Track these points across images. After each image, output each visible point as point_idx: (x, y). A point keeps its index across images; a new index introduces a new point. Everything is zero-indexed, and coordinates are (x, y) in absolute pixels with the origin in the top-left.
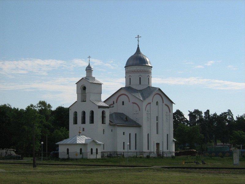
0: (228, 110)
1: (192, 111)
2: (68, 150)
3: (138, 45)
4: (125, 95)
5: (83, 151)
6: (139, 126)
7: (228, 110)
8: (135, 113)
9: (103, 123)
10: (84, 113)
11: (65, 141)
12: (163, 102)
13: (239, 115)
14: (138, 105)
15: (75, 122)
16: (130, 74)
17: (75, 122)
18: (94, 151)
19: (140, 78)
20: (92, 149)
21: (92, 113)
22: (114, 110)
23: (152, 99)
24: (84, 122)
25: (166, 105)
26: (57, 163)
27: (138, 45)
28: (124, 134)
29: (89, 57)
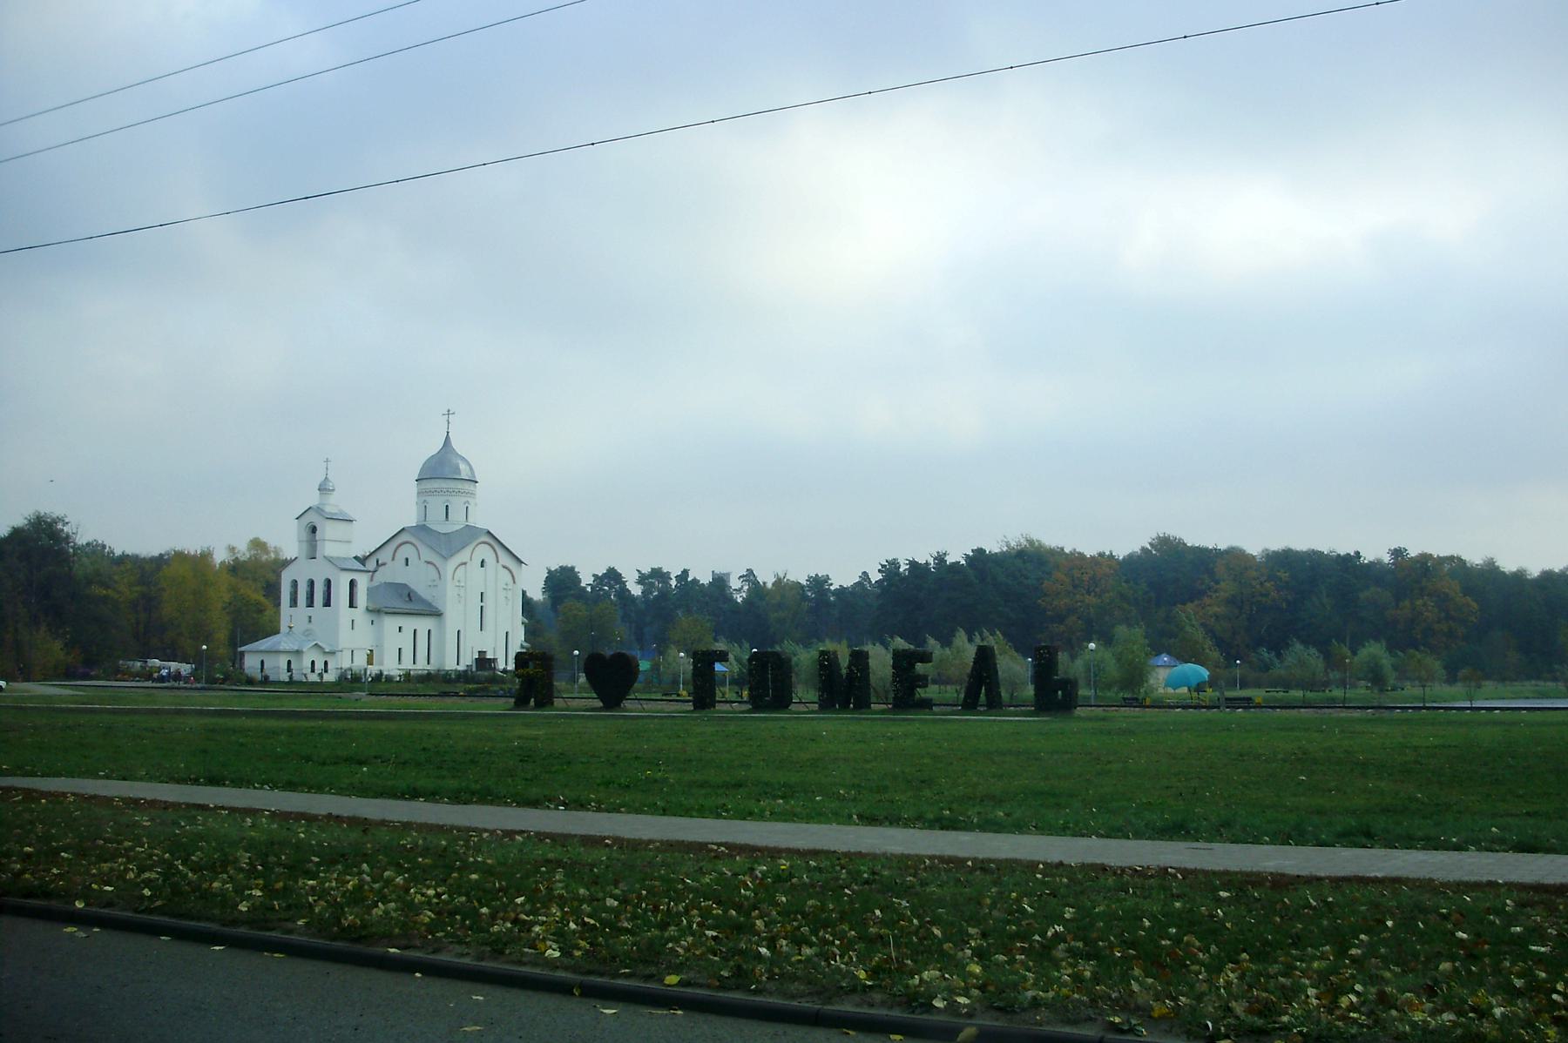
0: (748, 570)
1: (646, 570)
2: (262, 662)
3: (448, 432)
4: (411, 543)
5: (292, 666)
6: (436, 614)
7: (748, 570)
8: (430, 583)
9: (351, 605)
10: (311, 583)
11: (264, 644)
12: (498, 562)
13: (787, 577)
14: (435, 566)
15: (294, 603)
16: (426, 498)
17: (294, 603)
18: (319, 666)
19: (447, 506)
20: (313, 662)
21: (328, 583)
22: (383, 576)
23: (471, 549)
24: (310, 603)
25: (504, 567)
26: (1300, 712)
27: (448, 432)
28: (400, 631)
29: (327, 461)
